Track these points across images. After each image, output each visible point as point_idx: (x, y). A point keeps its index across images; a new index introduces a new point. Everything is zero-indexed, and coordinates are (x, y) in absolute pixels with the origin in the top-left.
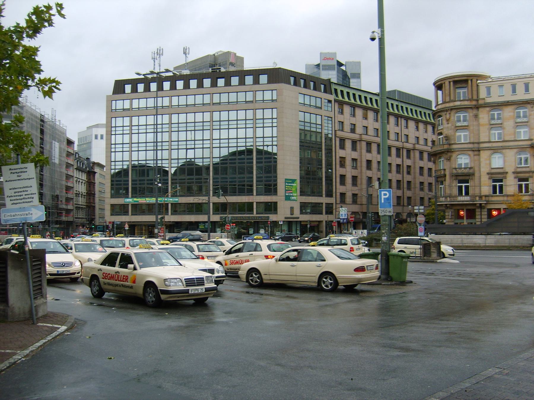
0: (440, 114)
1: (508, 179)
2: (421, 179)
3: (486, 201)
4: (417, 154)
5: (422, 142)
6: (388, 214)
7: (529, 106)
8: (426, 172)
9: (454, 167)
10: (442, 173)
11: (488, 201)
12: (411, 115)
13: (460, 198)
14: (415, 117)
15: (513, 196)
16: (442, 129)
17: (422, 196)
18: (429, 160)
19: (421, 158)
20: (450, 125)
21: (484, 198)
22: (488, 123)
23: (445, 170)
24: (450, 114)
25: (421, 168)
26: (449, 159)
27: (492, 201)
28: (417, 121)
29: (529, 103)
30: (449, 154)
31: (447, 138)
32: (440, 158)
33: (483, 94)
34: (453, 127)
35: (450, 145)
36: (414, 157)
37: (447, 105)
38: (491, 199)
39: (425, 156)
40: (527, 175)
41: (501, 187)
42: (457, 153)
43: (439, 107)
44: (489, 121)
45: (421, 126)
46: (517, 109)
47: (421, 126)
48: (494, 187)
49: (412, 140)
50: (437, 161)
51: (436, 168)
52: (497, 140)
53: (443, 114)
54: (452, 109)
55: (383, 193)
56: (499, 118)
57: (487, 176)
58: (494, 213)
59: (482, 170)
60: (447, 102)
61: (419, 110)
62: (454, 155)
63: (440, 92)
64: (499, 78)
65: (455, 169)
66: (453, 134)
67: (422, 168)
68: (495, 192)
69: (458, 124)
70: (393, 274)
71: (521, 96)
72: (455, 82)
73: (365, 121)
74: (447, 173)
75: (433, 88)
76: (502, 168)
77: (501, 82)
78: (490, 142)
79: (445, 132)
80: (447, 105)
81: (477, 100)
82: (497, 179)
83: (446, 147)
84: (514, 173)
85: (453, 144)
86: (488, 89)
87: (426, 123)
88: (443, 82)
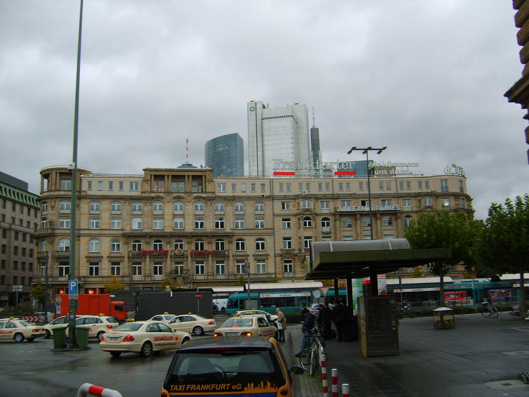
0: (45, 200)
1: (103, 262)
2: (15, 258)
3: (84, 281)
4: (13, 234)
5: (17, 222)
6: (75, 298)
7: (122, 201)
8: (20, 251)
9: (56, 249)
10: (45, 255)
11: (85, 282)
12: (9, 196)
13: (61, 279)
14: (13, 198)
15: (107, 277)
16: (46, 215)
17: (15, 275)
18: (31, 242)
19: (16, 238)
20: (54, 212)
21: (82, 279)
22: (88, 212)
23: (47, 252)
24: (55, 201)
25: (16, 248)
26: (52, 243)
27: (89, 281)
28: (14, 202)
29: (122, 199)
30: (52, 238)
31: (51, 223)
32: (43, 241)
33: (85, 187)
34: (57, 214)
35: (54, 229)
36: (10, 237)
37: (53, 193)
38: (88, 279)
39: (28, 238)
40: (118, 260)
41: (97, 269)
42: (60, 237)
43: (45, 194)
44: (89, 211)
45: (18, 207)
46: (112, 203)
47: (18, 207)
48: (91, 269)
49: (8, 220)
50: (39, 244)
51: (38, 249)
52: (95, 228)
53: (48, 201)
54: (57, 198)
55: (72, 283)
56: (97, 210)
57: (86, 260)
58: (90, 292)
59: (81, 253)
60: (53, 191)
61: (16, 191)
62: (57, 239)
63: (46, 181)
64: (99, 175)
65: (58, 251)
66: (56, 220)
67: (17, 247)
68: (91, 273)
69: (62, 211)
70: (78, 342)
71: (116, 192)
72: (61, 174)
73: (13, 213)
74: (50, 255)
75: (40, 176)
76: (98, 253)
77: (101, 177)
78: (89, 229)
79: (50, 218)
80: (53, 193)
81: (80, 192)
82: (94, 261)
83: (49, 231)
84: (108, 257)
85: (56, 229)
86: (90, 183)
87: (22, 204)
88: (50, 172)
